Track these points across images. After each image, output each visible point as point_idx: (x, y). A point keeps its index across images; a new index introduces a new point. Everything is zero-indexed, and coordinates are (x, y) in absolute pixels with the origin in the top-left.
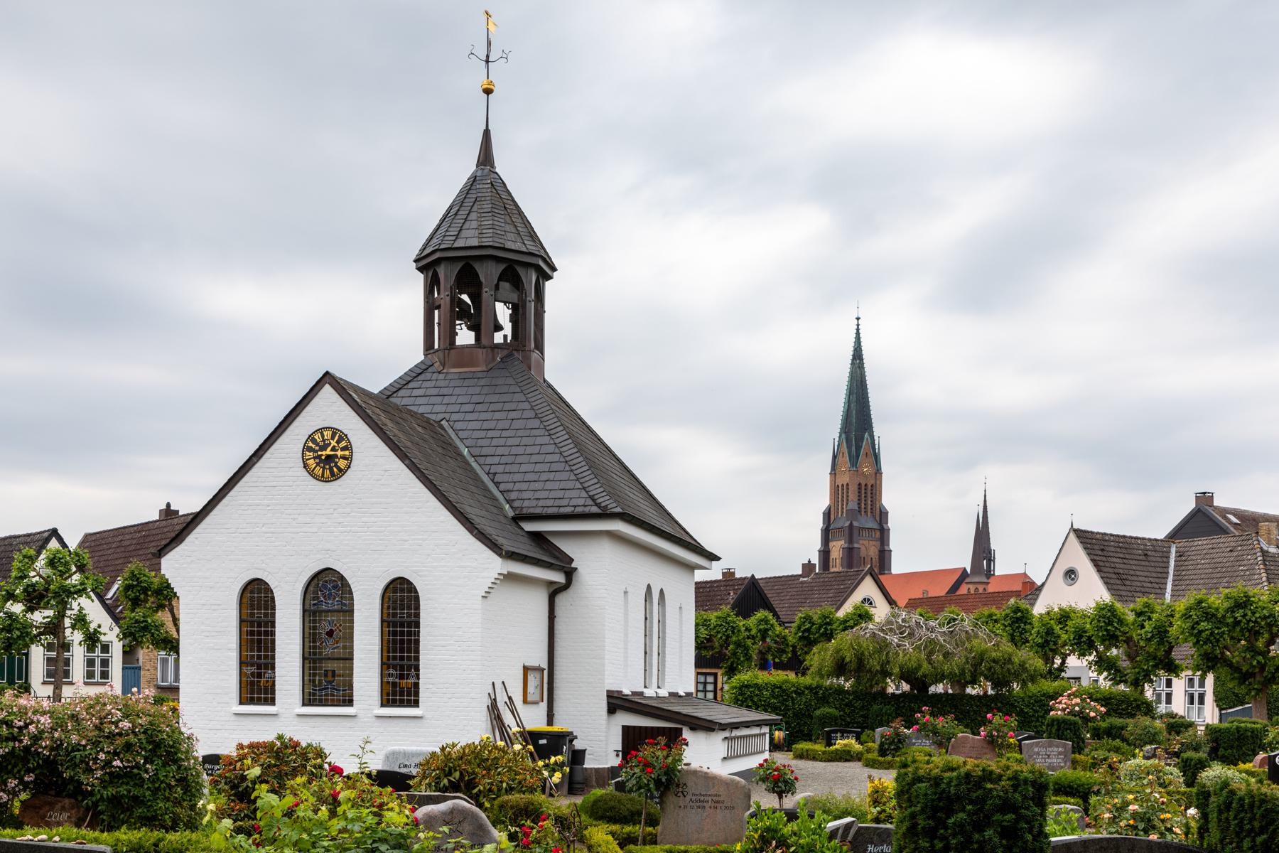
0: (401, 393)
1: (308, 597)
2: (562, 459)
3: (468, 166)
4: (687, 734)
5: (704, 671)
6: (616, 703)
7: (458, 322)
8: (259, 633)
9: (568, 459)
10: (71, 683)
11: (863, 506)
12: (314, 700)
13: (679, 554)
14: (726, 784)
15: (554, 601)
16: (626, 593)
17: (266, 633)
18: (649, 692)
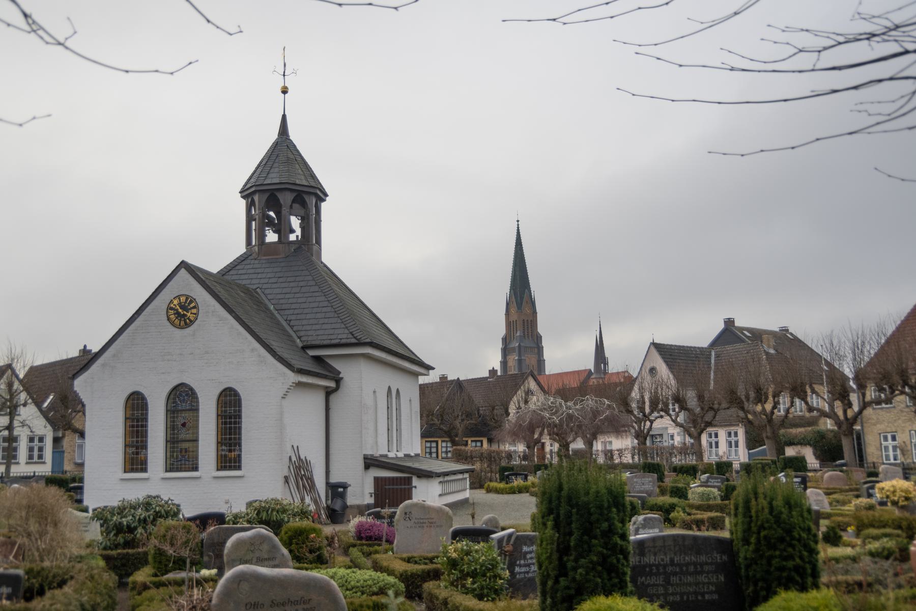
0: (231, 273)
1: (170, 401)
2: (333, 310)
3: (274, 136)
4: (415, 481)
5: (430, 439)
6: (370, 463)
7: (267, 229)
8: (137, 426)
9: (336, 310)
10: (18, 463)
11: (526, 333)
12: (173, 468)
13: (417, 369)
14: (439, 511)
15: (329, 399)
16: (374, 392)
17: (142, 426)
18: (391, 455)
